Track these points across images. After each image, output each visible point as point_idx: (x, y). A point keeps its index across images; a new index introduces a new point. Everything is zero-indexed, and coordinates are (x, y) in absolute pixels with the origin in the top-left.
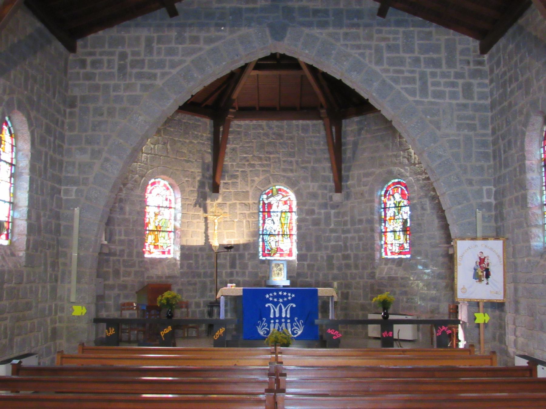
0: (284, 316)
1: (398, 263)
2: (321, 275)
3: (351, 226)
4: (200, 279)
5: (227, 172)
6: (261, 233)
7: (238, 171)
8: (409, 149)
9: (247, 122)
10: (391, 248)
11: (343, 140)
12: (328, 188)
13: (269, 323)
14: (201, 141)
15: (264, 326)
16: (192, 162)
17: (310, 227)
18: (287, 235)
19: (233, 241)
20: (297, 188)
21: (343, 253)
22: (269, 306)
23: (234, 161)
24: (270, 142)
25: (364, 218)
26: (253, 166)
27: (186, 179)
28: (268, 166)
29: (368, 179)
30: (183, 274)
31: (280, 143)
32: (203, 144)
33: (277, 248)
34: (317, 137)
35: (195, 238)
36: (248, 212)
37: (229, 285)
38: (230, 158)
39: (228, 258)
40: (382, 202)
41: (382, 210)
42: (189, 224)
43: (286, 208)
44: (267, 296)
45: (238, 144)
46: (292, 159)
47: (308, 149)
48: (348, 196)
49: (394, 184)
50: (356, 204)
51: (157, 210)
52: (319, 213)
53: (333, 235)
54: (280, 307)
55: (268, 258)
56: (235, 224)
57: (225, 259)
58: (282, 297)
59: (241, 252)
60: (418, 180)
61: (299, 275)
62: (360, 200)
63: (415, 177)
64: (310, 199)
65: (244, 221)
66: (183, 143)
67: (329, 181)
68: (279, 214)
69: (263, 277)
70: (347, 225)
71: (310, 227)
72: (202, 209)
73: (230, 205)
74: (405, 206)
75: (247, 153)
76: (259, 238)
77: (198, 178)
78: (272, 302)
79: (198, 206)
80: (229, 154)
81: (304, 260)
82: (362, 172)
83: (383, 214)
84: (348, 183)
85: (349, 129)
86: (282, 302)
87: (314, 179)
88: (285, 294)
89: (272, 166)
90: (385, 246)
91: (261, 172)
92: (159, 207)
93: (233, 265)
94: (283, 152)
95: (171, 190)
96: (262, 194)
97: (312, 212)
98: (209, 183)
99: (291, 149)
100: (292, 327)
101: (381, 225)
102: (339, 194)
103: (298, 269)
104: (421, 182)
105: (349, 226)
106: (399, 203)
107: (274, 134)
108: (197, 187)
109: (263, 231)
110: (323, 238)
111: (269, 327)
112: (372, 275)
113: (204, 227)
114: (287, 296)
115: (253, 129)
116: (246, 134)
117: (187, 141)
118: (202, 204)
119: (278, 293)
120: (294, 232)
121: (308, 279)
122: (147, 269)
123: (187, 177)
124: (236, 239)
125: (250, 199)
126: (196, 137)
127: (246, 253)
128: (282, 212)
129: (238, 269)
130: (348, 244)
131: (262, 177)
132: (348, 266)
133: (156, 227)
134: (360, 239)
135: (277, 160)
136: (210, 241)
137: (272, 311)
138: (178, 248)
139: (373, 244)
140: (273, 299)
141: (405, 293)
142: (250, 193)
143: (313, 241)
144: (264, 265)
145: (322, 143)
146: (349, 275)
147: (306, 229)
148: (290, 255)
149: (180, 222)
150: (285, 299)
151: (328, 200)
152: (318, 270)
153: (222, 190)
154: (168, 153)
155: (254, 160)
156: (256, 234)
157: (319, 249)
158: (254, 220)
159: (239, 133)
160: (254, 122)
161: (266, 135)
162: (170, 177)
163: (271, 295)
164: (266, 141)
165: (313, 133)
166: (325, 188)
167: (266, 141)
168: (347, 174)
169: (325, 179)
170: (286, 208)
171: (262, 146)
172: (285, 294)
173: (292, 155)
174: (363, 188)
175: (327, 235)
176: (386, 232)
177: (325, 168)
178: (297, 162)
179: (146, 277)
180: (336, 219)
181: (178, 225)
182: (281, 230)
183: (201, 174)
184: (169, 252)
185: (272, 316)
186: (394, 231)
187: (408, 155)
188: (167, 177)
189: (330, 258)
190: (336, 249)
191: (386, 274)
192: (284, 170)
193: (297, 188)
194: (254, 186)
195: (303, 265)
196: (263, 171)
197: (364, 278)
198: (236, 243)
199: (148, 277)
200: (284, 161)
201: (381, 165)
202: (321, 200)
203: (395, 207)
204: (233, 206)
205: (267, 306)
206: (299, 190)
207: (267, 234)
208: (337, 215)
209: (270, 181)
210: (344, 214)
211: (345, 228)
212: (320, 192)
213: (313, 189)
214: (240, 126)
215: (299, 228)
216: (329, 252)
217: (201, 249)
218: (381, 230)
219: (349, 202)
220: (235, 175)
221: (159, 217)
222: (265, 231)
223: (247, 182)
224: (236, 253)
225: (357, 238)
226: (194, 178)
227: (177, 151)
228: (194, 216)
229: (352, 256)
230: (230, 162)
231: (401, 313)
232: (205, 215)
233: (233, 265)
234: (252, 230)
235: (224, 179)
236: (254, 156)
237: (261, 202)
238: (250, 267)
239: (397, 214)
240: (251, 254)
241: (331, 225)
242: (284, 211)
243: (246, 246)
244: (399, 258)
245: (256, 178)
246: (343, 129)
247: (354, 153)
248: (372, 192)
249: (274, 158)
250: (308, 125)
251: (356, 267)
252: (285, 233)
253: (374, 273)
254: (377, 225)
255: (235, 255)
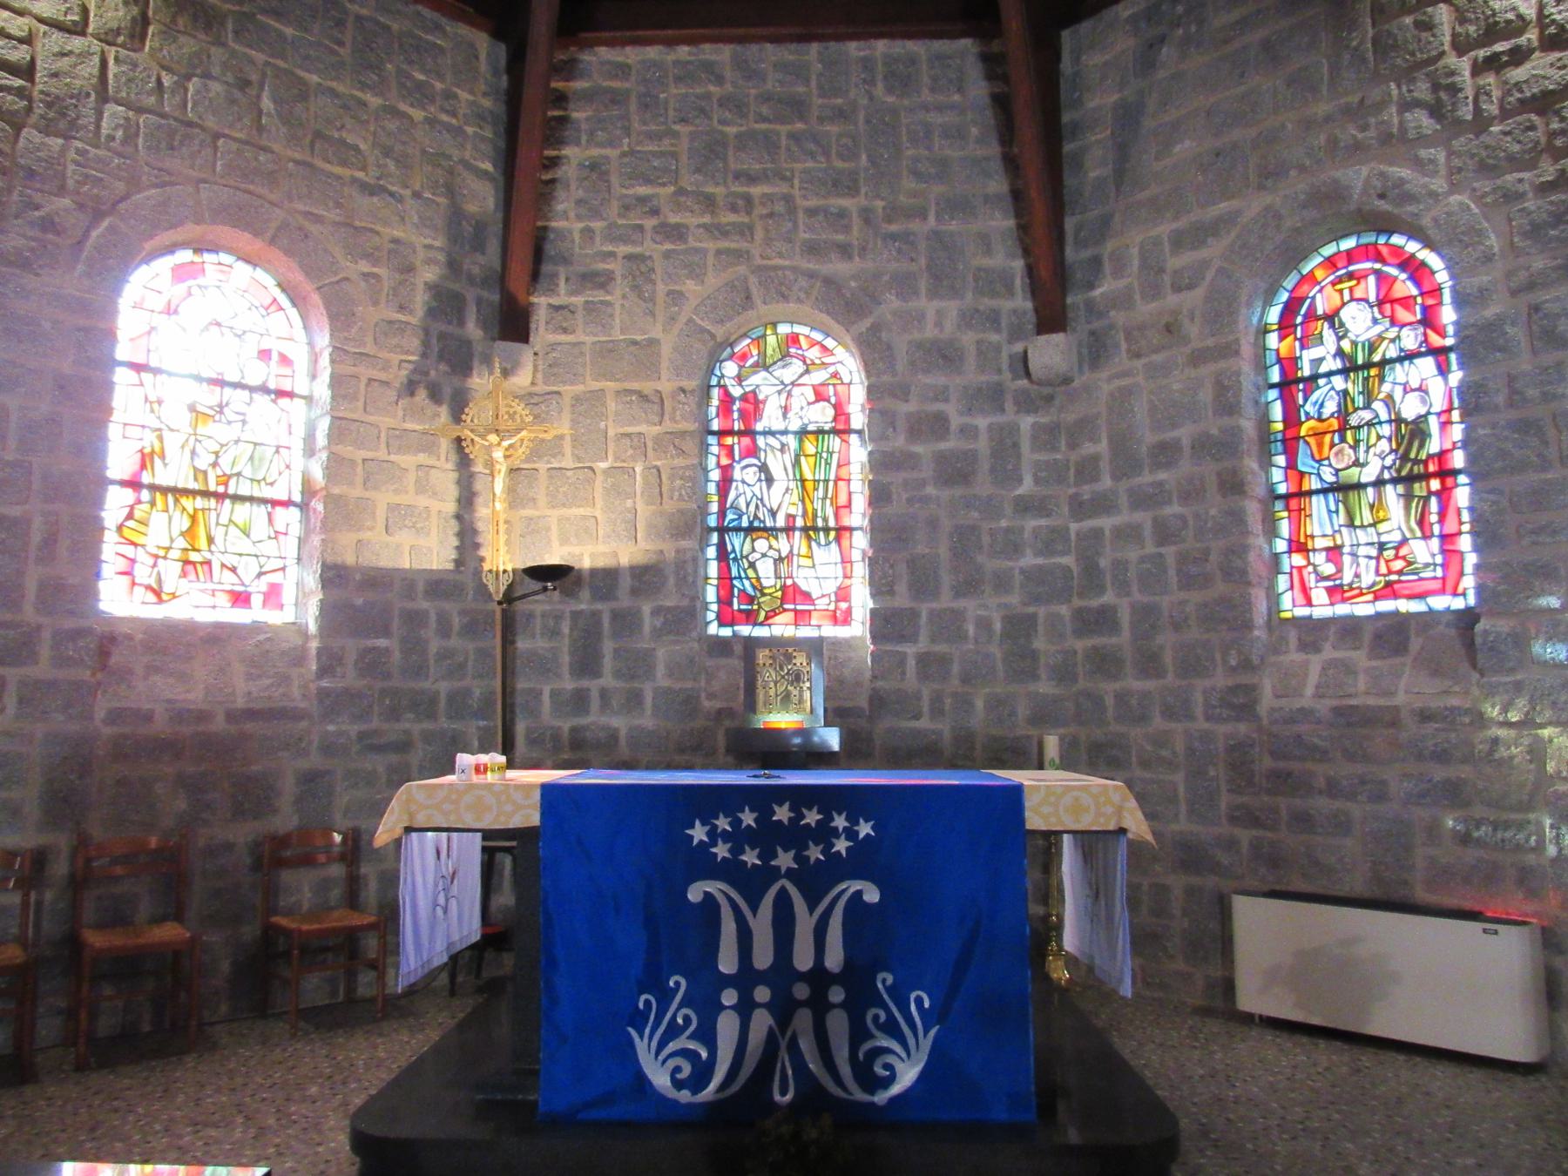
0: (803, 959)
1: (1378, 637)
2: (979, 704)
3: (1116, 478)
4: (427, 725)
5: (566, 260)
6: (712, 521)
7: (612, 254)
8: (1443, 53)
9: (653, 52)
10: (1329, 569)
11: (1066, 117)
12: (1004, 322)
13: (709, 1010)
14: (445, 118)
15: (673, 1031)
16: (401, 200)
17: (930, 490)
18: (827, 530)
19: (585, 556)
20: (866, 323)
21: (1077, 602)
22: (708, 896)
23: (596, 214)
24: (752, 135)
25: (1184, 434)
26: (676, 233)
27: (364, 266)
28: (746, 231)
29: (1204, 253)
30: (332, 703)
31: (791, 136)
32: (458, 132)
33: (784, 588)
34: (952, 107)
35: (404, 538)
36: (656, 429)
37: (464, 759)
38: (579, 202)
39: (566, 630)
40: (1271, 358)
41: (1273, 394)
42: (375, 474)
43: (822, 415)
44: (699, 833)
45: (611, 144)
46: (845, 202)
47: (916, 160)
48: (1096, 352)
49: (1331, 263)
50: (1140, 379)
51: (208, 397)
52: (968, 432)
53: (1031, 523)
54: (783, 901)
55: (745, 630)
56: (600, 478)
57: (554, 633)
58: (795, 836)
59: (624, 601)
60: (1511, 197)
61: (879, 701)
62: (1158, 358)
63: (1484, 185)
64: (926, 371)
65: (638, 469)
66: (353, 107)
67: (1010, 292)
68: (792, 441)
69: (720, 712)
70: (1095, 478)
71: (930, 490)
72: (444, 411)
73: (577, 399)
74: (1410, 356)
75: (648, 181)
76: (704, 544)
77: (430, 274)
78: (731, 871)
79: (422, 395)
80: (573, 187)
81: (902, 638)
82: (1164, 229)
83: (1277, 411)
84: (1097, 292)
85: (1094, 60)
86: (790, 874)
87: (942, 281)
88: (812, 817)
89: (759, 234)
90: (1298, 559)
91: (710, 260)
92: (220, 383)
93: (587, 664)
94: (805, 171)
95: (293, 313)
96: (714, 360)
97: (937, 426)
98: (479, 302)
99: (841, 157)
100: (859, 1034)
101: (1267, 464)
102: (1058, 338)
103: (875, 677)
104: (1530, 204)
105: (1107, 482)
106: (1372, 347)
107: (767, 98)
108: (420, 312)
109: (722, 514)
110: (986, 539)
111: (707, 1035)
112: (1240, 702)
113: (453, 492)
114: (825, 833)
115: (679, 80)
116: (649, 104)
117: (374, 101)
118: (447, 391)
119: (765, 815)
120: (858, 515)
121: (924, 723)
122: (124, 674)
123: (367, 256)
124: (602, 548)
125: (664, 374)
126: (421, 94)
127: (646, 609)
128: (803, 433)
129: (608, 680)
130: (1104, 563)
131: (713, 280)
132: (1104, 663)
133: (200, 474)
134: (1164, 534)
135: (780, 208)
136: (482, 552)
137: (729, 927)
138: (312, 581)
139: (1241, 550)
140: (737, 850)
141: (1453, 794)
142: (666, 350)
143: (943, 551)
144: (723, 661)
145: (974, 131)
146: (1109, 701)
147: (909, 501)
148: (841, 618)
149: (324, 455)
150: (815, 853)
151: (1007, 375)
152: (966, 679)
153: (542, 333)
154: (260, 129)
155: (679, 207)
156: (690, 525)
157: (969, 586)
158: (680, 462)
159: (617, 98)
160: (683, 51)
161: (735, 104)
162: (272, 241)
163: (723, 823)
164: (731, 130)
165: (933, 90)
166: (993, 319)
167: (731, 130)
168: (1085, 254)
169: (994, 283)
170: (822, 415)
171: (711, 152)
172: (812, 817)
173: (845, 184)
174: (1172, 300)
175: (1004, 523)
176: (1301, 494)
177: (992, 239)
178: (867, 216)
179: (100, 714)
180: (1043, 457)
181: (318, 474)
182: (796, 510)
183: (441, 257)
184: (272, 595)
185: (727, 963)
186: (1343, 489)
187: (1436, 87)
188: (258, 244)
189: (1019, 627)
190: (1043, 585)
191: (1318, 695)
192: (812, 249)
193: (866, 323)
194: (683, 319)
195: (902, 660)
196: (719, 252)
197: (1190, 717)
198: (601, 563)
199: (115, 716)
200: (812, 212)
201: (1270, 174)
202: (971, 375)
203: (1344, 372)
204: (589, 404)
205: (695, 894)
206: (875, 328)
207: (738, 529)
208: (1047, 436)
209: (748, 298)
210: (1082, 429)
211: (1086, 491)
212: (968, 339)
213: (939, 324)
214: (623, 70)
215: (879, 496)
216: (1014, 599)
217: (437, 586)
218: (1271, 488)
219: (1104, 375)
220: (596, 274)
221: (218, 431)
222: (730, 516)
223: (652, 300)
224: (599, 606)
225: (1148, 531)
226: (410, 269)
227: (318, 135)
228: (400, 441)
229: (1125, 617)
230: (579, 218)
231: (1421, 895)
232: (457, 431)
233: (587, 664)
234: (669, 506)
235: (552, 291)
236: (681, 192)
237: (715, 392)
238: (660, 670)
239: (1360, 401)
240: (669, 609)
241: (1020, 481)
242: (811, 428)
243: (645, 577)
244: (1379, 616)
245: (690, 286)
246: (1066, 65)
247: (1122, 152)
248: (1222, 311)
249: (769, 198)
250: (913, 60)
251: (1150, 664)
252: (820, 523)
253: (1251, 690)
254: (1252, 464)
255: (595, 616)
